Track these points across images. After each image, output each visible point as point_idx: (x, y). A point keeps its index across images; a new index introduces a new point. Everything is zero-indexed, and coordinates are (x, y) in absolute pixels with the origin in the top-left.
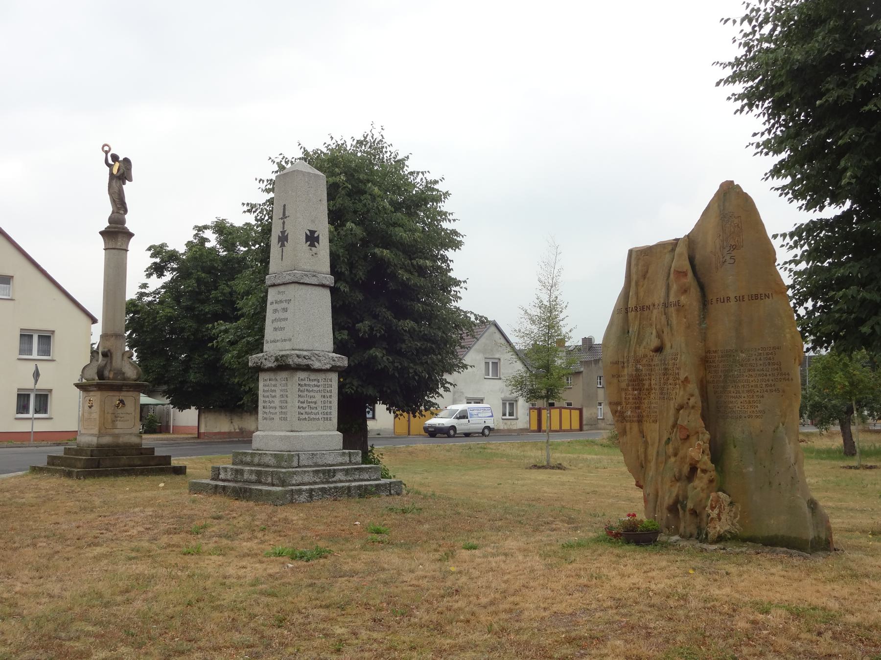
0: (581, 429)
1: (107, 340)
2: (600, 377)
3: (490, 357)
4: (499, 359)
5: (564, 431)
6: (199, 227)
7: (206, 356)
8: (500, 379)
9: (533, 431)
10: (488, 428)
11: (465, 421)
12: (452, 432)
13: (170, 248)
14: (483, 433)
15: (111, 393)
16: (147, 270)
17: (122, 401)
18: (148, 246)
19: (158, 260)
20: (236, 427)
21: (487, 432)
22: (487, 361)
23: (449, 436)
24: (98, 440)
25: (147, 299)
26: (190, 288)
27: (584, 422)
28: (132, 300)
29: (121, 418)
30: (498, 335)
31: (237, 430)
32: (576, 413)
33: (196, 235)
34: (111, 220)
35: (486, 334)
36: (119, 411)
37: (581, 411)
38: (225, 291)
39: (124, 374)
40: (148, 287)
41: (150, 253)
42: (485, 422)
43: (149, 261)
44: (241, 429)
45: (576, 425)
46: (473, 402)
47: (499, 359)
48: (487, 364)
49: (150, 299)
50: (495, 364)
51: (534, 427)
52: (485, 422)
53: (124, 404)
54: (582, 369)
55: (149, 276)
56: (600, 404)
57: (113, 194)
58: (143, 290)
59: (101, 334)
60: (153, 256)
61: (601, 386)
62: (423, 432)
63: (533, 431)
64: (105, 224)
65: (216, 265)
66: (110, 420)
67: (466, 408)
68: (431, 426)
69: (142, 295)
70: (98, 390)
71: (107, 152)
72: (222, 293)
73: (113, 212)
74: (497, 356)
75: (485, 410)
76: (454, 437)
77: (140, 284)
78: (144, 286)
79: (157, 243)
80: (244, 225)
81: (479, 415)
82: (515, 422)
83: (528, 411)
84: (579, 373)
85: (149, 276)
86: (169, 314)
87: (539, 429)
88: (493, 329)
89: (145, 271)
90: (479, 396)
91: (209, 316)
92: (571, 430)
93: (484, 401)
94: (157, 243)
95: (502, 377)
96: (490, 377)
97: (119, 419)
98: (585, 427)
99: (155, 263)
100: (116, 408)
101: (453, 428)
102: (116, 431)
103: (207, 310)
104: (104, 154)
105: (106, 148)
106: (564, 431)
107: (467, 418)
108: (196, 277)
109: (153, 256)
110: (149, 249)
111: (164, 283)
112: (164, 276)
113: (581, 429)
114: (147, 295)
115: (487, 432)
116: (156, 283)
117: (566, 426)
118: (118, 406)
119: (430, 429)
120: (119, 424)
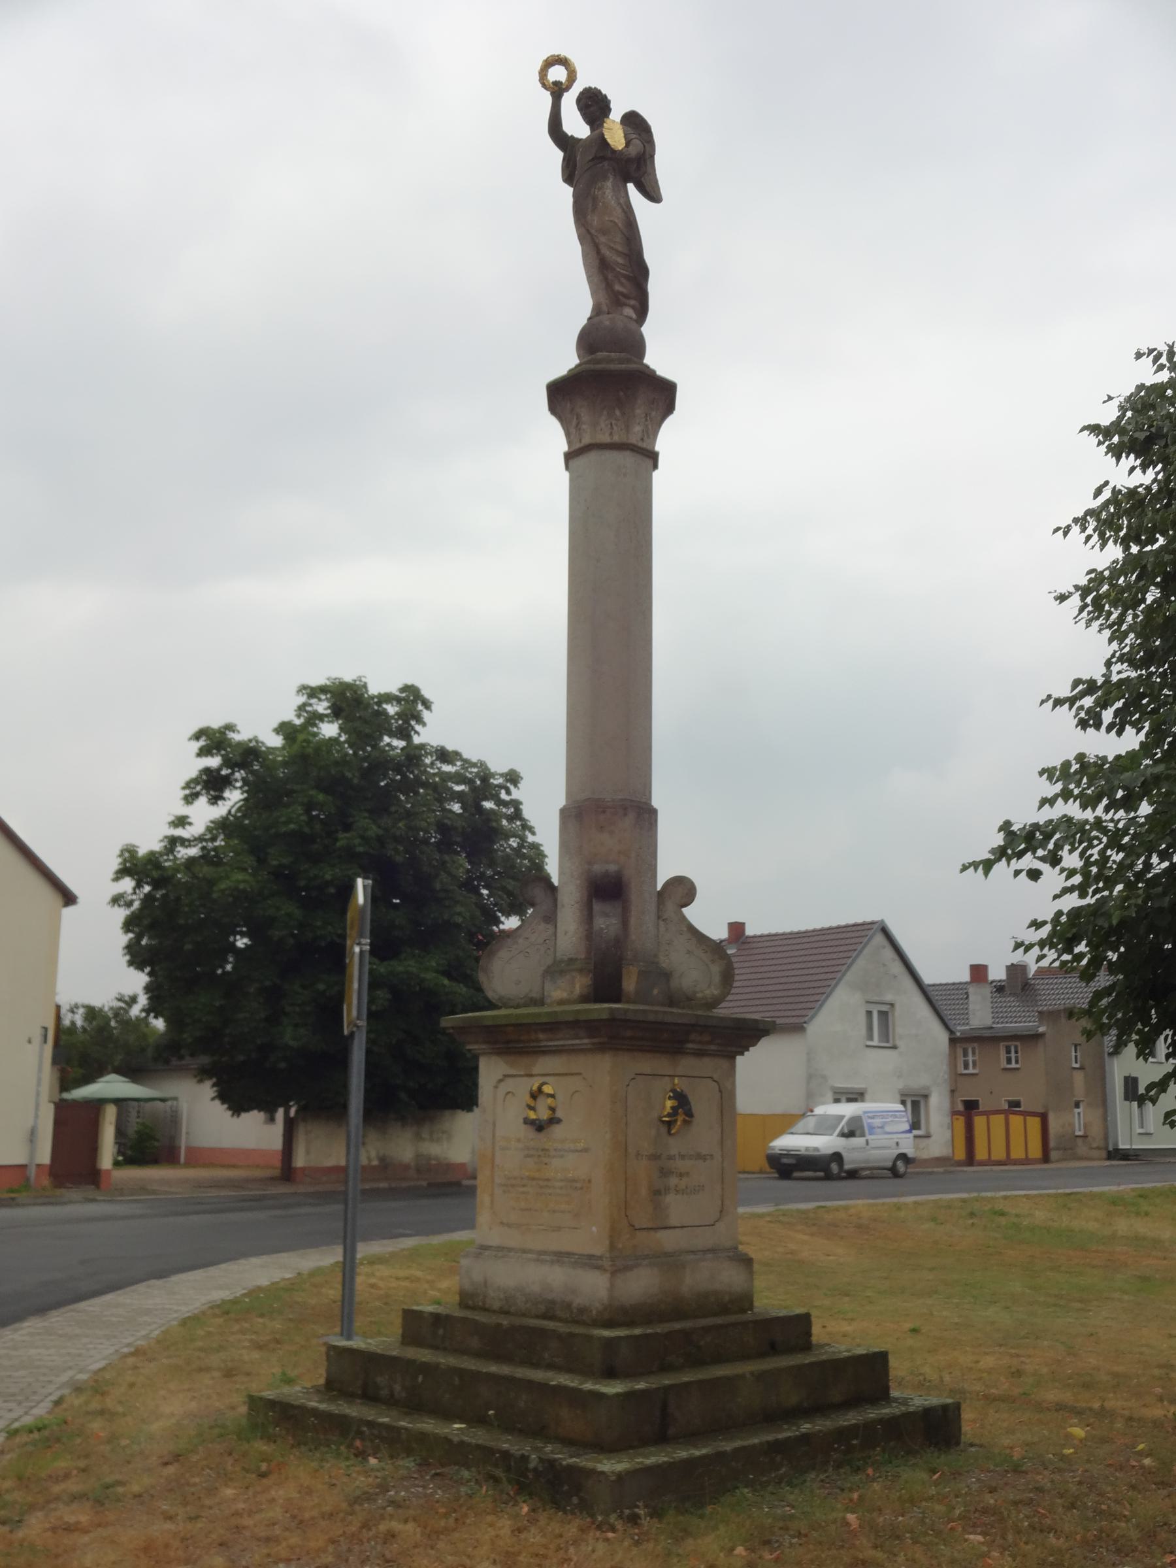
0: (1046, 1159)
1: (601, 828)
2: (1076, 1046)
3: (876, 999)
4: (892, 1005)
5: (1016, 1162)
6: (312, 689)
7: (321, 987)
8: (894, 1047)
9: (959, 1164)
10: (903, 1157)
11: (857, 1141)
12: (834, 1167)
13: (242, 735)
14: (894, 1172)
15: (647, 1064)
16: (187, 785)
17: (681, 1099)
18: (195, 728)
19: (214, 762)
20: (373, 1154)
21: (901, 1166)
22: (871, 1007)
23: (829, 1177)
24: (612, 1285)
25: (184, 853)
26: (292, 826)
27: (1052, 1144)
28: (152, 853)
29: (681, 1175)
30: (889, 953)
31: (375, 1163)
32: (1034, 1123)
33: (301, 708)
34: (588, 341)
35: (865, 952)
36: (675, 1146)
37: (1044, 1118)
38: (370, 833)
39: (667, 975)
40: (190, 824)
41: (196, 745)
42: (897, 1144)
43: (194, 765)
44: (382, 1159)
45: (1036, 1151)
46: (844, 1099)
47: (892, 1005)
48: (869, 1013)
49: (193, 851)
50: (883, 1015)
51: (961, 1155)
52: (897, 1144)
53: (689, 1114)
54: (1041, 1030)
55: (190, 799)
56: (1077, 1105)
57: (604, 232)
58: (179, 832)
59: (561, 801)
60: (203, 752)
61: (1077, 1066)
62: (767, 1167)
63: (959, 1164)
64: (566, 360)
65: (349, 775)
66: (644, 1192)
67: (859, 1113)
68: (788, 1154)
69: (173, 842)
70: (601, 1048)
71: (557, 91)
72: (362, 837)
73: (597, 311)
74: (889, 997)
75: (896, 1116)
76: (839, 1178)
77: (171, 818)
78: (181, 821)
79: (216, 724)
80: (402, 690)
81: (888, 1129)
82: (926, 1141)
83: (947, 1120)
84: (1037, 1037)
85: (190, 799)
86: (242, 886)
87: (970, 1159)
88: (879, 939)
89: (184, 788)
90: (855, 1084)
91: (332, 890)
92: (1027, 1161)
93: (867, 1097)
94: (216, 723)
95: (898, 1043)
96: (875, 1043)
97: (673, 1181)
98: (1054, 1155)
99: (207, 771)
100: (664, 1129)
101: (837, 1157)
102: (668, 1240)
103: (328, 877)
104: (547, 98)
105: (557, 74)
106: (1016, 1162)
107: (863, 1135)
108: (306, 800)
109: (203, 752)
110: (197, 736)
111: (212, 822)
112: (224, 799)
113: (1046, 1159)
114: (184, 842)
115: (901, 1166)
116: (204, 814)
117: (1017, 1153)
118: (669, 1124)
119: (785, 1161)
120: (677, 1208)
